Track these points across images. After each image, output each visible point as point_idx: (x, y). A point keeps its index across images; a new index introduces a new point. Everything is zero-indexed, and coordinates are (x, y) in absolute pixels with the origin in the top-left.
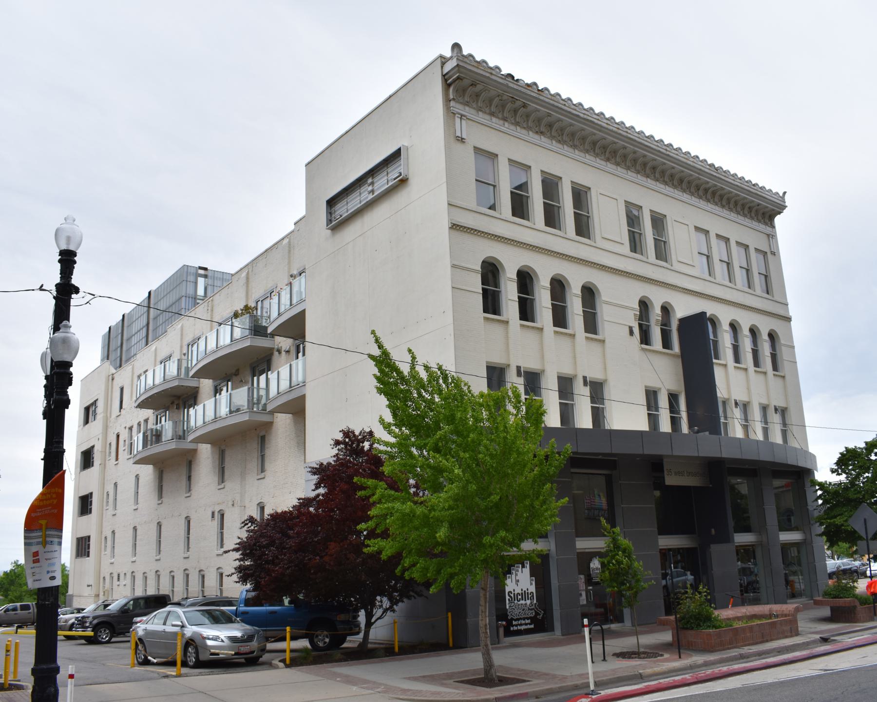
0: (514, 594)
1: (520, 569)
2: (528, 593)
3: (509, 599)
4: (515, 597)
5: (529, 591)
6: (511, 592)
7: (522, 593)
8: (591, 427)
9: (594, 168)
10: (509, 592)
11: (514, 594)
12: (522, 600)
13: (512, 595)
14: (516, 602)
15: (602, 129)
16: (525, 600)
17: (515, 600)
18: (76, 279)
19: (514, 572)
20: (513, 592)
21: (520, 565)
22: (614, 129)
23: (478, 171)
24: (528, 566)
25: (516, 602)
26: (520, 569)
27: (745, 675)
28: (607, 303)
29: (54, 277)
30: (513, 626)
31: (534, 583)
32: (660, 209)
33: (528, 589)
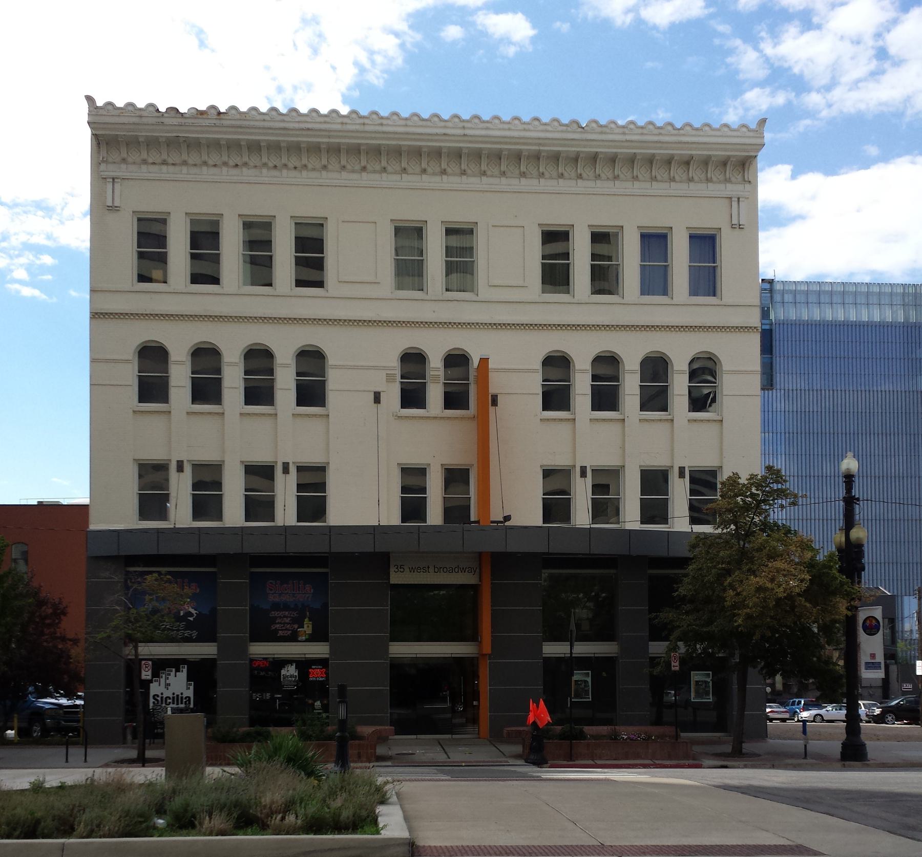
0: (162, 698)
1: (173, 674)
2: (182, 698)
3: (154, 702)
4: (285, 677)
5: (184, 696)
6: (158, 696)
7: (173, 698)
8: (93, 527)
9: (638, 306)
10: (154, 696)
11: (162, 698)
12: (173, 704)
13: (159, 699)
14: (164, 705)
15: (332, 133)
16: (177, 704)
17: (162, 703)
18: (855, 492)
19: (164, 676)
20: (160, 696)
21: (174, 670)
22: (358, 127)
23: (139, 267)
24: (185, 670)
25: (164, 705)
26: (173, 674)
27: (487, 843)
28: (336, 367)
29: (842, 493)
30: (157, 729)
31: (192, 688)
32: (460, 216)
33: (182, 694)
